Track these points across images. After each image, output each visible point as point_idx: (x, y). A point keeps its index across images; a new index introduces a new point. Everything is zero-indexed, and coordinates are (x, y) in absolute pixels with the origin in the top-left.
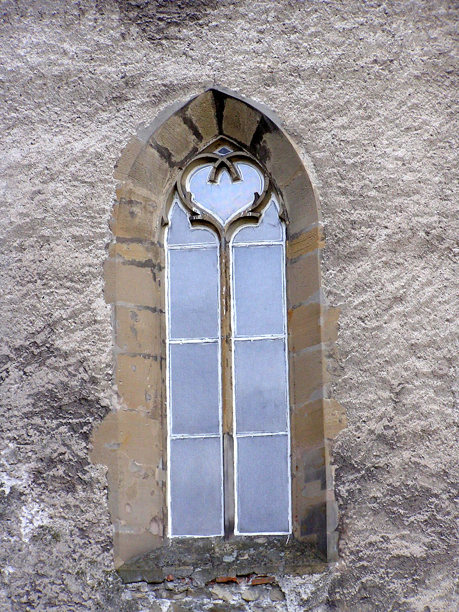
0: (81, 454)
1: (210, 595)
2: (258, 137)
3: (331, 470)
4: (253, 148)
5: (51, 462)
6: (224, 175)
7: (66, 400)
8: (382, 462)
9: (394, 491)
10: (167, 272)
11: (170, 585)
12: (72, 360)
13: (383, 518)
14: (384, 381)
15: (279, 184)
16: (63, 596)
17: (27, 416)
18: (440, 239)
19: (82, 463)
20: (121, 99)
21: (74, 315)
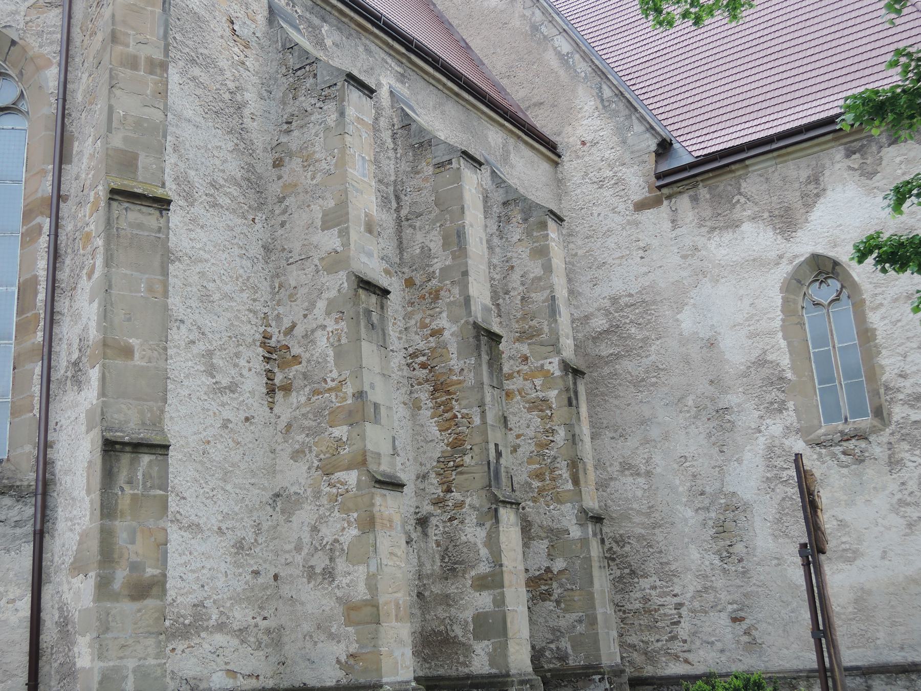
0: (783, 399)
1: (841, 446)
2: (834, 268)
3: (882, 391)
4: (833, 273)
5: (772, 403)
6: (823, 284)
7: (774, 379)
8: (902, 385)
9: (909, 395)
10: (807, 326)
11: (824, 444)
12: (774, 364)
13: (906, 406)
14: (898, 353)
15: (844, 285)
16: (784, 453)
17: (760, 387)
18: (646, 248)
19: (784, 401)
20: (778, 264)
21: (773, 347)
